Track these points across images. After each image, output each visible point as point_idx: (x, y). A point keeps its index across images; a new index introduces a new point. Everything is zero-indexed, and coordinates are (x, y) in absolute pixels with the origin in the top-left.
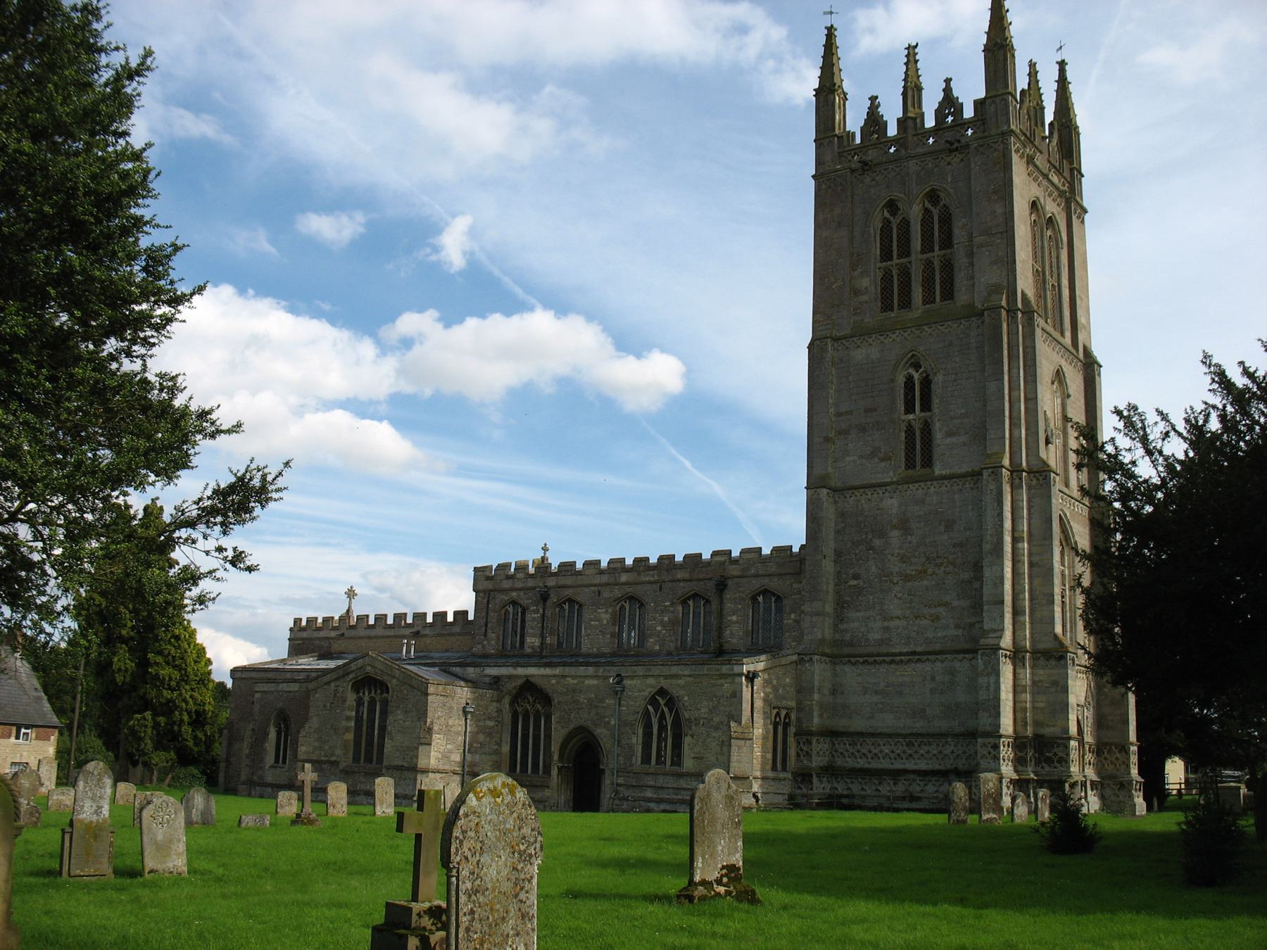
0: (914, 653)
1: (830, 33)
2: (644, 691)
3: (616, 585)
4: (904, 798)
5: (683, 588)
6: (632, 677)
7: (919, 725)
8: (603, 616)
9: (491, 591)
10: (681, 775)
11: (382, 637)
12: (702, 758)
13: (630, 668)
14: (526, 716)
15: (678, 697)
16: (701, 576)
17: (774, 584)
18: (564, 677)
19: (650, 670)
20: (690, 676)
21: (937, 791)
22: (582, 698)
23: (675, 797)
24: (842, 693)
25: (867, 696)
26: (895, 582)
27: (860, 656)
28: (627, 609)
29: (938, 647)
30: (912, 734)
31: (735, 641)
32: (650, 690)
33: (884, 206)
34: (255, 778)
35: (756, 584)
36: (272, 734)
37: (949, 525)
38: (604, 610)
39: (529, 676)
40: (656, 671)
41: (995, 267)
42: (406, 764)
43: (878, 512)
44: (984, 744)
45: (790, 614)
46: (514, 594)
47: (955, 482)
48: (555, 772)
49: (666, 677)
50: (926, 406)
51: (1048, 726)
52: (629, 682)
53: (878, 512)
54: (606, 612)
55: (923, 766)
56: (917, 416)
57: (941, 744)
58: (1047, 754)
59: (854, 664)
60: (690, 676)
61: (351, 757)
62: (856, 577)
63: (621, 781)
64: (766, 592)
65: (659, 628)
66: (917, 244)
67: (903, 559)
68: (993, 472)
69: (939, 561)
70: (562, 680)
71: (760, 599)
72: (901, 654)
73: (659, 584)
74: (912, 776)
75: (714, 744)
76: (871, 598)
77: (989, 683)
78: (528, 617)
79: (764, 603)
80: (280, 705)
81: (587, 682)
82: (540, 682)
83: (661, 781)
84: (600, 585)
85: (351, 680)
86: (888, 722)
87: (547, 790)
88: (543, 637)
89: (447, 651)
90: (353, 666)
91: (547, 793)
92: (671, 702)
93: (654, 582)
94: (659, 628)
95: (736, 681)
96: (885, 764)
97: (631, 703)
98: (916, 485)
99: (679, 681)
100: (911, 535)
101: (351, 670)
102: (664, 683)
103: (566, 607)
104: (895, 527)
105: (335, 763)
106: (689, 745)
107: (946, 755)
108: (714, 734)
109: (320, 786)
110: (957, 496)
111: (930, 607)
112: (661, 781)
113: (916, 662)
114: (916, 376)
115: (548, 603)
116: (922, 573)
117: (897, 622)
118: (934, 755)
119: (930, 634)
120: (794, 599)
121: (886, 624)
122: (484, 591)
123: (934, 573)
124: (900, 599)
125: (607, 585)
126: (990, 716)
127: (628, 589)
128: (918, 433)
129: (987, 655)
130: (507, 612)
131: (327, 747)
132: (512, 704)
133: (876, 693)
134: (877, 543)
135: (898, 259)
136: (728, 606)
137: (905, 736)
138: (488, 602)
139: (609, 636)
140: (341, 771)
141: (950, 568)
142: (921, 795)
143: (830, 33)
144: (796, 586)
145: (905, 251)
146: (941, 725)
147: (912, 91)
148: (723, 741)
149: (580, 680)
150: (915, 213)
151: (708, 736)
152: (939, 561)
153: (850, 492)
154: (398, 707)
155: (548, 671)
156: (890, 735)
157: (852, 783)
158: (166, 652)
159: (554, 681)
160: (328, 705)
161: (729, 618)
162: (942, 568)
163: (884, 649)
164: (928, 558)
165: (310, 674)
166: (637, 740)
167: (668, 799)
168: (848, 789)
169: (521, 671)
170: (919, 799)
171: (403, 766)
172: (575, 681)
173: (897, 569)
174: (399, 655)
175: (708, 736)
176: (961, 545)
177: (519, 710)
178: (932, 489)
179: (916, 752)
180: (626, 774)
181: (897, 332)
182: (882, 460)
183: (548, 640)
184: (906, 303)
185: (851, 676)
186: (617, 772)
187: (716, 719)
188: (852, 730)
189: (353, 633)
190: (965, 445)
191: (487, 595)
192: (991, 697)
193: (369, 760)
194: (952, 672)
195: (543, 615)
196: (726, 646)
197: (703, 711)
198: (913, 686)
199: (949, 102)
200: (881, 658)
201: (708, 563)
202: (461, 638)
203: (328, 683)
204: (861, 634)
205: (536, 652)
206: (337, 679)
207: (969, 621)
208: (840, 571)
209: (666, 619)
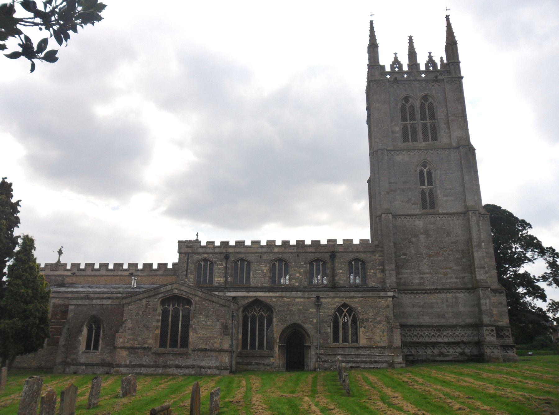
0: (436, 289)
1: (371, 23)
2: (334, 304)
3: (271, 253)
4: (439, 355)
5: (311, 257)
6: (325, 298)
7: (442, 322)
8: (264, 268)
9: (190, 253)
10: (359, 348)
11: (105, 276)
12: (371, 339)
13: (325, 293)
14: (253, 318)
15: (355, 308)
16: (321, 251)
17: (361, 256)
18: (282, 297)
19: (337, 294)
20: (361, 297)
21: (455, 352)
22: (294, 308)
23: (356, 359)
24: (401, 307)
25: (415, 308)
26: (424, 257)
27: (410, 290)
28: (277, 266)
29: (448, 287)
30: (439, 326)
31: (341, 282)
32: (337, 304)
33: (402, 99)
34: (68, 360)
35: (352, 256)
36: (85, 331)
37: (449, 234)
38: (264, 265)
39: (258, 297)
40: (342, 294)
41: (460, 130)
42: (208, 348)
43: (413, 226)
44: (487, 329)
45: (371, 270)
46: (206, 255)
47: (433, 217)
48: (277, 349)
49: (347, 298)
50: (430, 183)
51: (499, 321)
52: (324, 300)
53: (413, 226)
54: (266, 266)
55: (446, 340)
56: (426, 187)
57: (454, 330)
58: (501, 334)
59: (406, 294)
60: (361, 297)
61: (158, 344)
62: (405, 254)
63: (322, 352)
64: (357, 260)
65: (298, 275)
66: (418, 116)
67: (427, 247)
68: (473, 212)
69: (444, 249)
70: (280, 299)
71: (353, 263)
72: (430, 289)
73: (297, 254)
74: (442, 345)
75: (378, 331)
76: (413, 264)
77: (486, 302)
78: (215, 267)
79: (355, 264)
80: (94, 313)
81: (297, 300)
82: (268, 301)
83: (347, 351)
84: (262, 253)
85: (161, 298)
86: (426, 320)
87: (271, 359)
88: (226, 277)
89: (153, 284)
90: (163, 289)
91: (272, 360)
92: (351, 310)
93: (295, 253)
94: (298, 275)
95: (388, 300)
96: (427, 340)
97: (325, 311)
98: (431, 216)
99: (355, 300)
100: (431, 237)
101: (160, 291)
102: (345, 301)
103: (239, 263)
104: (422, 233)
105: (149, 349)
106: (363, 332)
107: (463, 335)
108: (378, 326)
109: (133, 363)
110: (451, 222)
111: (443, 269)
112: (347, 351)
113: (425, 294)
114: (425, 170)
115: (229, 261)
116: (437, 254)
117: (427, 275)
118: (451, 335)
119: (444, 281)
120: (373, 264)
121: (421, 276)
122: (185, 253)
123: (443, 254)
124: (428, 265)
125: (265, 253)
126: (488, 317)
127: (278, 255)
128: (427, 195)
129: (484, 290)
130: (200, 265)
131: (140, 339)
132: (243, 312)
133: (419, 307)
134: (414, 240)
135: (410, 121)
136: (337, 265)
137: (436, 327)
138: (188, 259)
139: (268, 278)
140: (152, 353)
141: (451, 252)
142: (448, 353)
143: (371, 23)
144: (373, 257)
145: (413, 118)
146: (453, 321)
147: (412, 54)
148: (383, 330)
149: (292, 299)
150: (417, 104)
151: (375, 327)
152: (444, 249)
153: (399, 217)
154: (201, 314)
155: (271, 294)
156: (429, 326)
157: (412, 349)
158: (24, 278)
159: (274, 300)
160: (141, 312)
161: (338, 271)
162: (447, 253)
163: (422, 287)
164: (440, 248)
165: (89, 295)
166: (330, 330)
167: (352, 360)
168: (410, 352)
169: (252, 294)
170: (447, 356)
171: (206, 349)
172: (289, 300)
173: (424, 252)
174: (129, 285)
175: (375, 327)
176: (455, 243)
177: (250, 315)
178: (438, 218)
179: (442, 334)
180: (324, 348)
181: (416, 151)
182: (413, 204)
183: (229, 279)
184: (415, 139)
185: (406, 299)
186: (320, 347)
187: (379, 319)
188: (409, 323)
189: (82, 273)
190: (453, 201)
191: (187, 255)
192: (488, 309)
193: (174, 344)
194: (456, 298)
195: (226, 267)
196: (337, 284)
197: (370, 314)
198: (438, 304)
199: (431, 61)
200: (420, 291)
201: (324, 246)
202: (163, 277)
203: (141, 299)
204: (409, 280)
205: (221, 285)
206: (149, 297)
207: (462, 275)
208: (396, 252)
209: (302, 270)
